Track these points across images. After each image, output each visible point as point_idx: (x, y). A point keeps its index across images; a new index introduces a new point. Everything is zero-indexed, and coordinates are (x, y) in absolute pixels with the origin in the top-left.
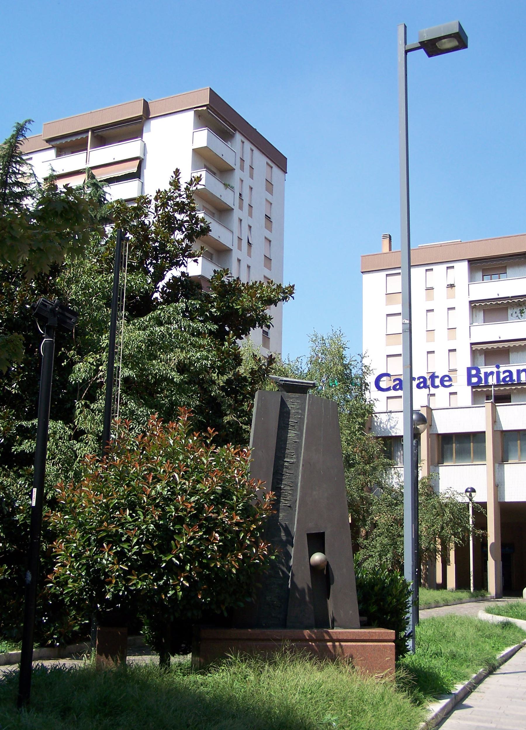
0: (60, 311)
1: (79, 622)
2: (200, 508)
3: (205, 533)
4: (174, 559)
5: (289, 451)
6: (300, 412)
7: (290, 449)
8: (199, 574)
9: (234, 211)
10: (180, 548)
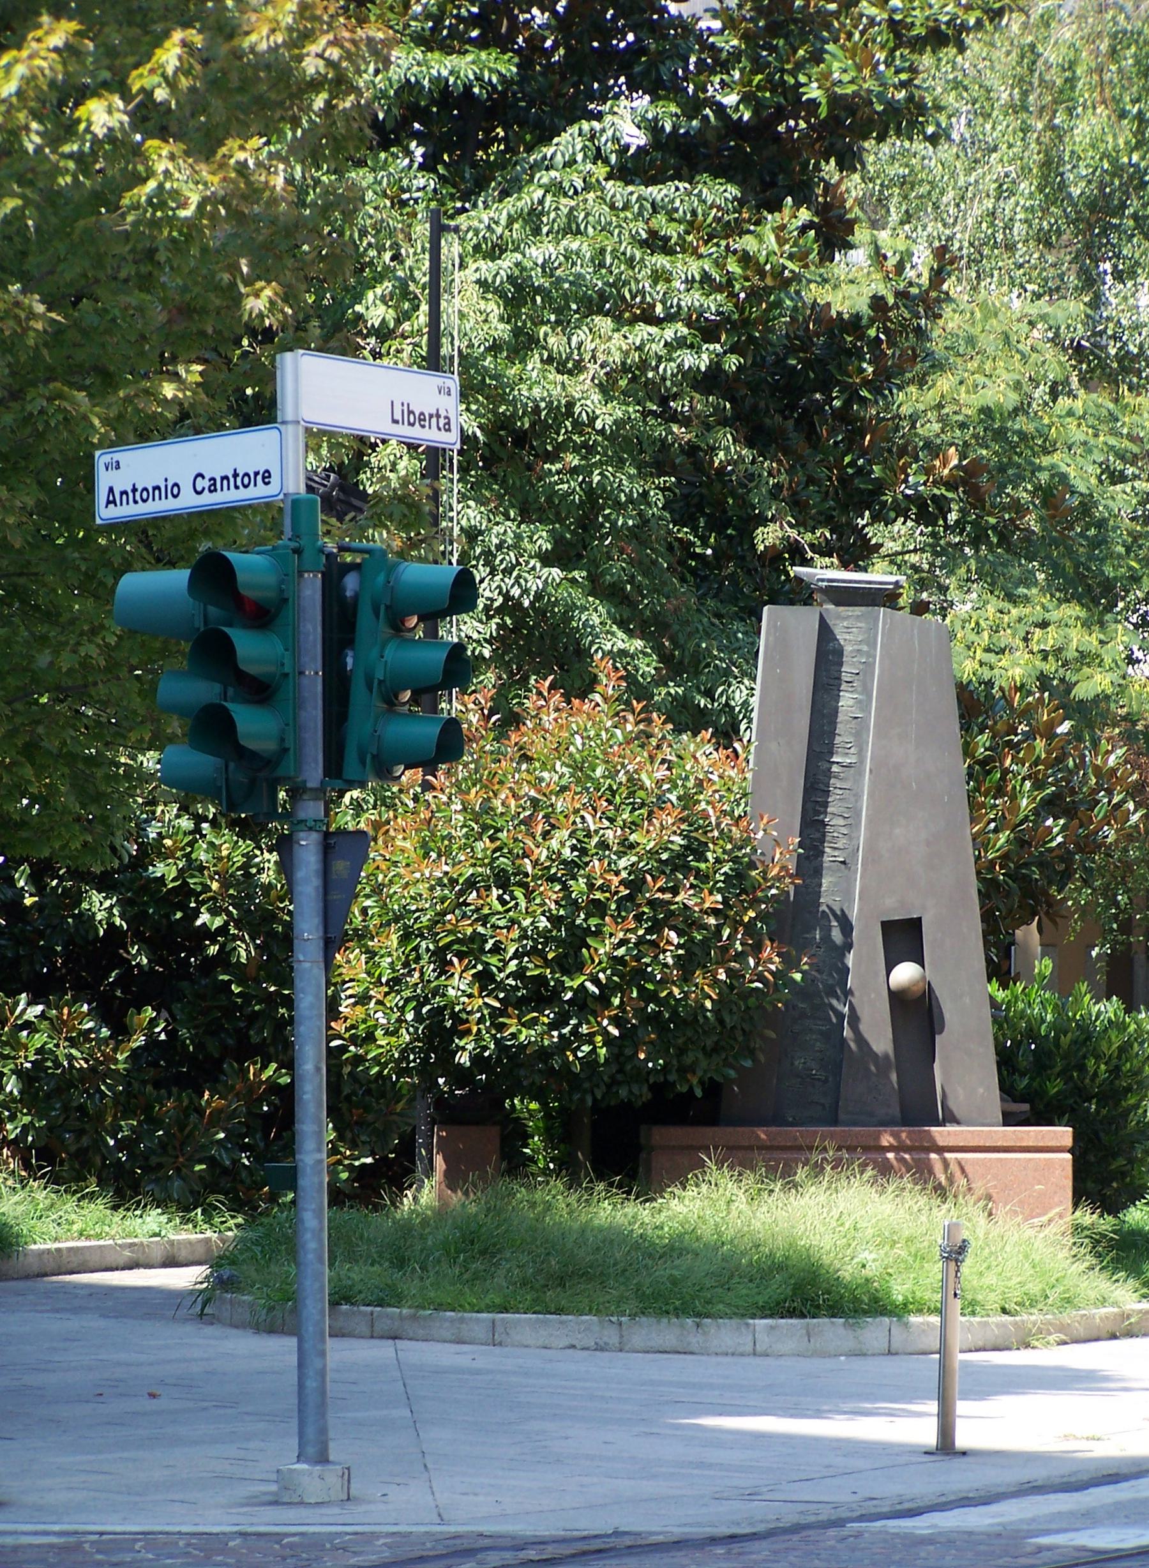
0: (342, 496)
1: (346, 1162)
2: (636, 884)
3: (648, 931)
4: (588, 984)
6: (865, 648)
7: (843, 735)
8: (640, 1012)
10: (600, 963)
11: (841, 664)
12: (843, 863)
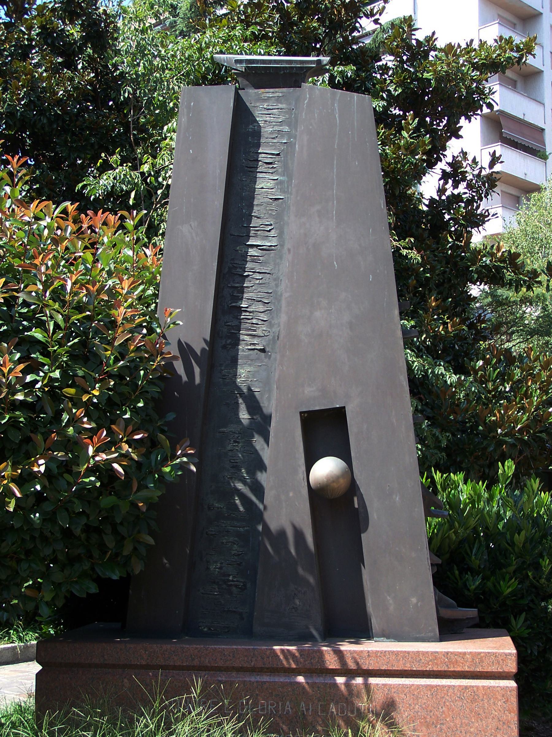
5: (260, 222)
9: (544, 16)
11: (258, 146)
12: (263, 351)
